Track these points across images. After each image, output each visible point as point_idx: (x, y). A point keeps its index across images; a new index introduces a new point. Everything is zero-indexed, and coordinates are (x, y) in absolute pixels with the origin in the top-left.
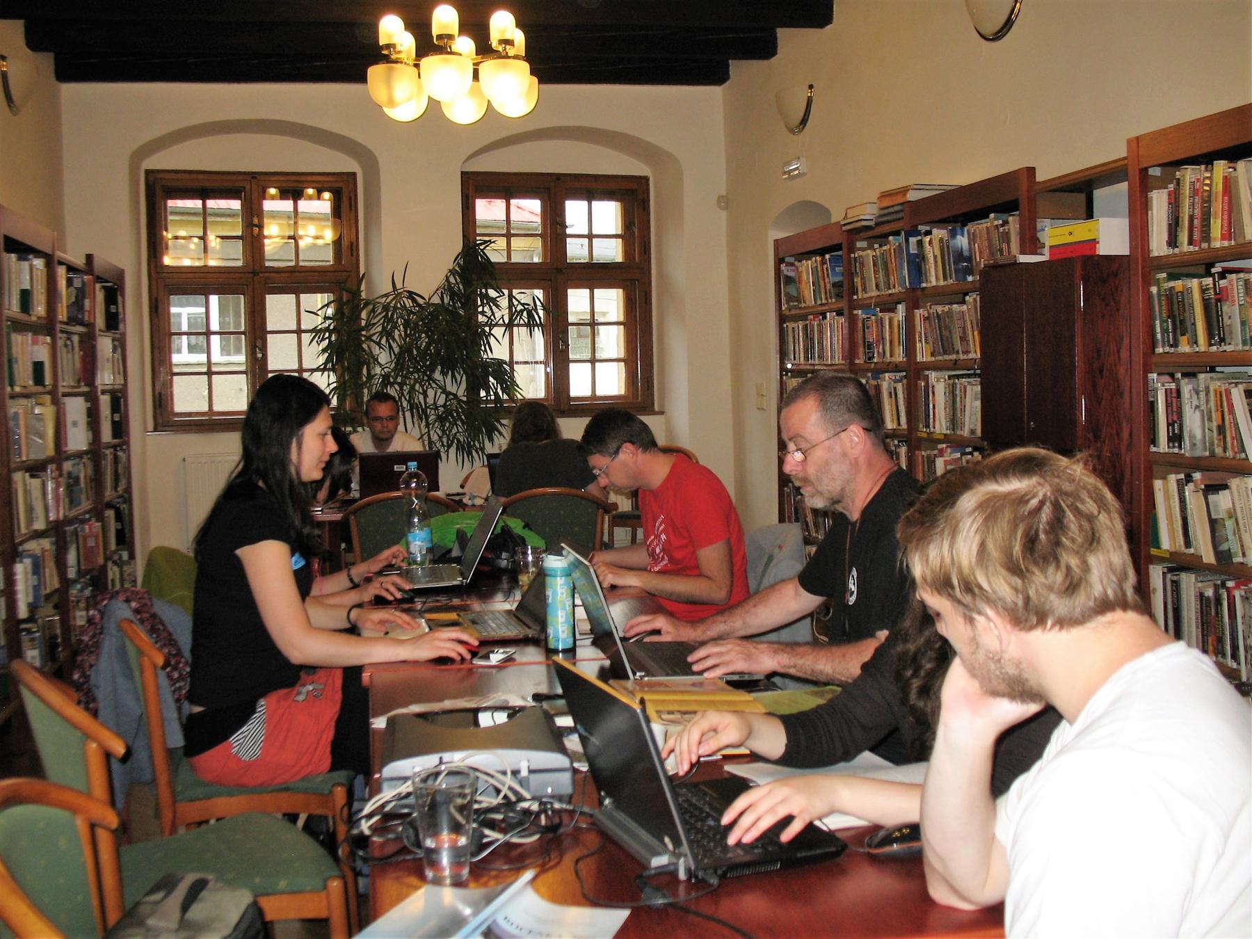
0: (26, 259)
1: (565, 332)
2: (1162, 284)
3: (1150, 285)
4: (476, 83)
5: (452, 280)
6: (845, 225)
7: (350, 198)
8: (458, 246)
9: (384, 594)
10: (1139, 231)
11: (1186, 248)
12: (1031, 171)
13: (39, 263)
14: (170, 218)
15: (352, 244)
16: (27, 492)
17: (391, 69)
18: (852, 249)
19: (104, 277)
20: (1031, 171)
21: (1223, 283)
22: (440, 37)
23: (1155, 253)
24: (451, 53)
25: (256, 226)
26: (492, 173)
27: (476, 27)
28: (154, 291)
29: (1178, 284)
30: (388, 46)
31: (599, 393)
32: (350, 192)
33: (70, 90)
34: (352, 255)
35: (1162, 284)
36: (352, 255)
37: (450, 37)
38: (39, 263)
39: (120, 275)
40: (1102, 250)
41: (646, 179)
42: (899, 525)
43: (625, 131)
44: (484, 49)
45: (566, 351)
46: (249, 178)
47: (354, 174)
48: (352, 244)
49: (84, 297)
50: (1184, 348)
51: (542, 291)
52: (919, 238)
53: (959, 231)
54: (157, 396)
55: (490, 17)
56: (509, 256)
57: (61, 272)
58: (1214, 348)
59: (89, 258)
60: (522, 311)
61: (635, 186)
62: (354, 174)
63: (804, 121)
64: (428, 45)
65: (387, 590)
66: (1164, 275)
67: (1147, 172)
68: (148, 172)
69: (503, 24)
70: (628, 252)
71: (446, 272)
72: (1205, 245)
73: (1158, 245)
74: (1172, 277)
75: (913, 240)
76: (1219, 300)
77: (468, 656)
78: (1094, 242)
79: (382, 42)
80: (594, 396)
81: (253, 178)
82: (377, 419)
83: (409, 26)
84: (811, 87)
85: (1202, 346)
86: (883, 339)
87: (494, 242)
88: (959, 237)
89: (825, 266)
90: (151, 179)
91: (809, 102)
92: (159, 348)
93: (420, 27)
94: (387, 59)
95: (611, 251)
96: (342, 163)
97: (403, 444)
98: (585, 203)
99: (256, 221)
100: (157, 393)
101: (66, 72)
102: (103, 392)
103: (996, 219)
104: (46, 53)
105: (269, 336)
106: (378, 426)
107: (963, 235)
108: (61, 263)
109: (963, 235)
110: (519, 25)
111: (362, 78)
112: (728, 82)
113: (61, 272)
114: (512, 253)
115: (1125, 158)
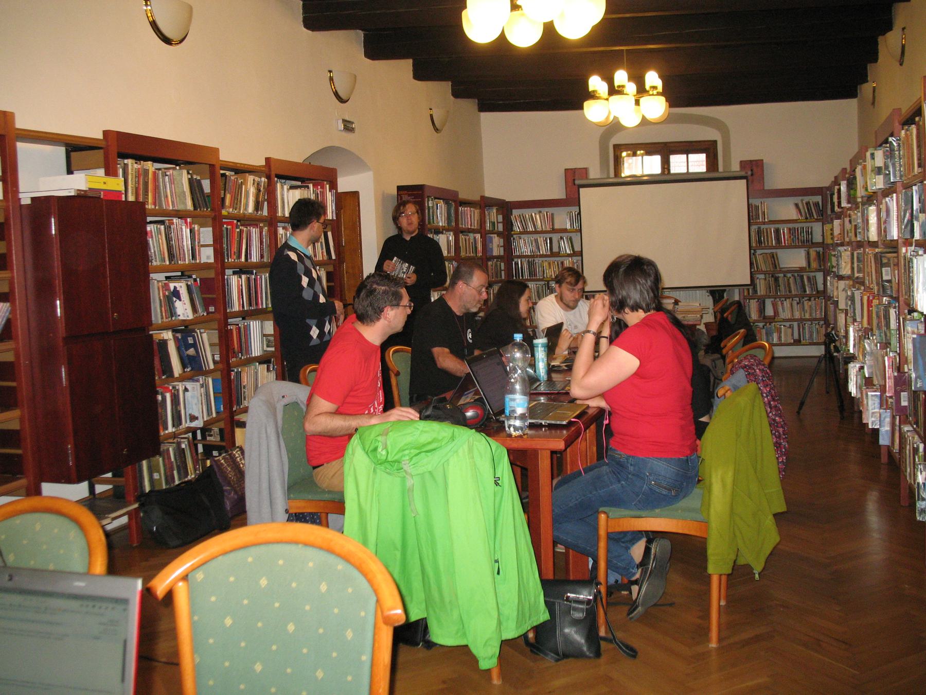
4: (638, 107)
16: (462, 239)
22: (619, 87)
24: (623, 94)
27: (638, 80)
30: (594, 91)
31: (691, 171)
33: (482, 114)
37: (623, 86)
42: (583, 641)
43: (718, 118)
44: (642, 90)
55: (590, 77)
64: (614, 91)
69: (653, 79)
80: (688, 173)
83: (631, 78)
93: (610, 80)
95: (674, 170)
104: (470, 100)
110: (660, 77)
111: (581, 108)
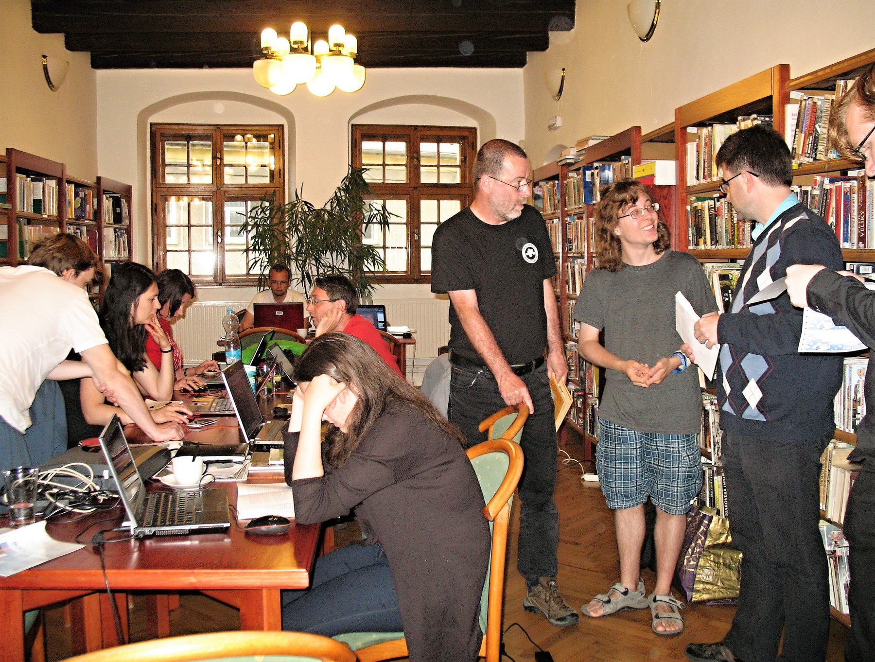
0: (41, 180)
1: (419, 228)
2: (693, 203)
3: (687, 204)
5: (338, 194)
6: (560, 161)
7: (280, 140)
8: (345, 171)
9: (188, 388)
10: (681, 171)
11: (702, 181)
12: (638, 129)
13: (53, 183)
14: (225, 149)
15: (280, 170)
17: (268, 63)
18: (565, 177)
19: (111, 190)
20: (638, 129)
21: (718, 204)
23: (689, 184)
25: (219, 158)
26: (380, 125)
28: (154, 199)
29: (699, 204)
30: (267, 48)
32: (279, 137)
33: (102, 74)
34: (280, 177)
35: (693, 203)
36: (280, 177)
38: (53, 183)
39: (128, 190)
40: (658, 182)
41: (475, 129)
45: (419, 241)
46: (215, 128)
47: (282, 126)
48: (280, 170)
49: (86, 204)
50: (702, 247)
51: (459, 202)
52: (593, 171)
53: (607, 167)
54: (155, 263)
55: (332, 25)
56: (439, 179)
57: (70, 189)
58: (713, 247)
59: (99, 179)
60: (377, 214)
61: (466, 134)
62: (282, 126)
63: (561, 91)
65: (189, 385)
66: (694, 198)
67: (686, 131)
68: (151, 124)
70: (463, 177)
71: (335, 189)
72: (709, 180)
73: (691, 181)
74: (699, 199)
75: (588, 173)
76: (716, 216)
77: (187, 421)
78: (652, 176)
79: (262, 46)
81: (218, 128)
82: (275, 282)
84: (564, 69)
85: (709, 247)
86: (577, 237)
87: (369, 170)
88: (607, 171)
89: (555, 188)
90: (154, 129)
91: (563, 77)
92: (157, 235)
94: (266, 56)
96: (277, 119)
97: (293, 298)
98: (436, 144)
99: (218, 155)
100: (155, 263)
101: (96, 64)
102: (106, 262)
103: (625, 159)
105: (422, 225)
106: (275, 286)
107: (609, 170)
108: (69, 182)
109: (609, 170)
112: (526, 66)
113: (70, 189)
114: (440, 173)
115: (674, 122)
